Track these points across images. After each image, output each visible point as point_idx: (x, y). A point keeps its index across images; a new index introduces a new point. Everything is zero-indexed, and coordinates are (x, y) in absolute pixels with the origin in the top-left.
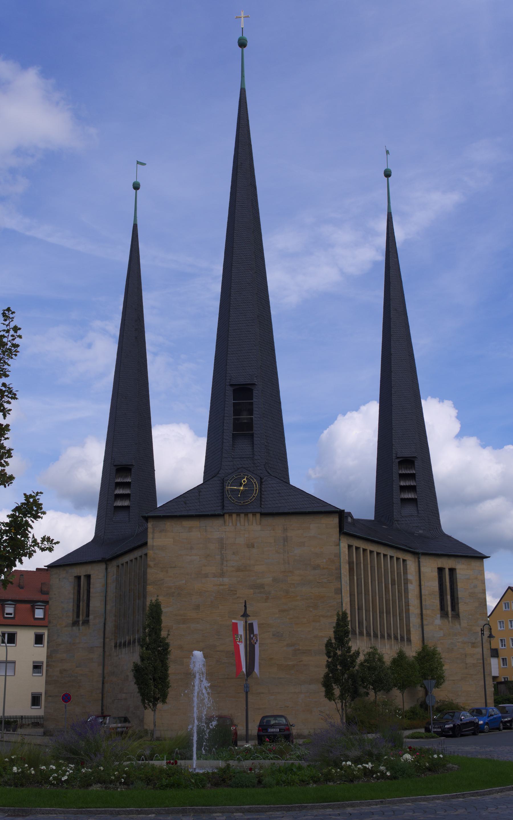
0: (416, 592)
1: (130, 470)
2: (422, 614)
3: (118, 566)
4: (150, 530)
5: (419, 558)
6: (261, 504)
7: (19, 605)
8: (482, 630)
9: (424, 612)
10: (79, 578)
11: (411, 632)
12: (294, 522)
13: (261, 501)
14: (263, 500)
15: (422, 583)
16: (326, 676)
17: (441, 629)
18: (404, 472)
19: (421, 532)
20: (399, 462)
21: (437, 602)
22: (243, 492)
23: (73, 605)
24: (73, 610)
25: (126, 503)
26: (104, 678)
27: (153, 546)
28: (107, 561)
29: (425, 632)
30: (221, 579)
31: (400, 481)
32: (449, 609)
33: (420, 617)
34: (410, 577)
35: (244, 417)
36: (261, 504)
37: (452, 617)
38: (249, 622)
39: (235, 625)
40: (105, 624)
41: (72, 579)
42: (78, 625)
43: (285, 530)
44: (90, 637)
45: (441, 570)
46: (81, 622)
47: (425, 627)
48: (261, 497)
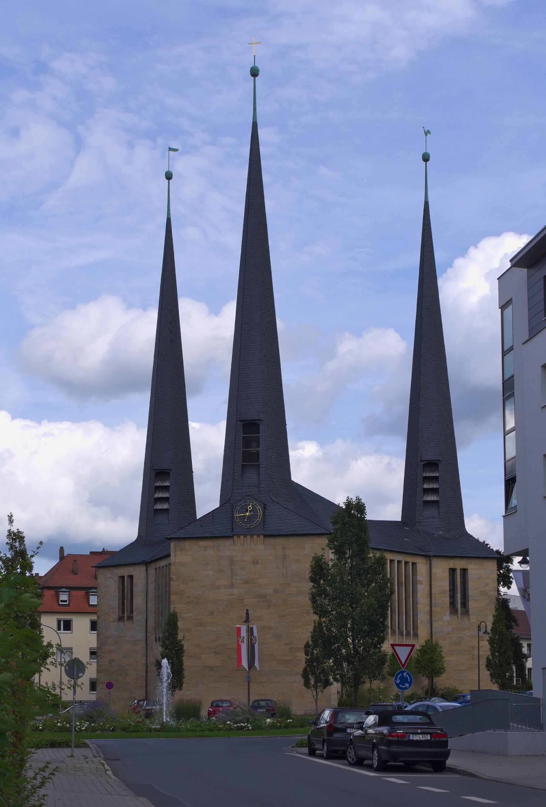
0: (427, 591)
1: (169, 474)
2: (431, 611)
3: (156, 569)
4: (172, 549)
5: (430, 560)
6: (264, 527)
7: (74, 592)
8: (479, 627)
9: (433, 609)
10: (122, 578)
11: (419, 628)
12: (292, 542)
13: (264, 524)
14: (266, 523)
15: (433, 583)
16: (305, 670)
17: (449, 625)
18: (427, 475)
19: (441, 533)
20: (424, 465)
21: (447, 600)
22: (249, 517)
23: (119, 603)
24: (119, 607)
25: (165, 506)
26: (147, 667)
27: (175, 563)
28: (147, 564)
29: (433, 627)
30: (231, 590)
31: (423, 484)
32: (459, 606)
33: (429, 613)
34: (419, 578)
35: (253, 450)
36: (264, 527)
37: (461, 614)
38: (251, 626)
39: (239, 630)
40: (146, 620)
41: (116, 579)
42: (124, 621)
43: (284, 549)
44: (134, 631)
45: (452, 571)
46: (126, 618)
47: (434, 623)
48: (264, 521)
